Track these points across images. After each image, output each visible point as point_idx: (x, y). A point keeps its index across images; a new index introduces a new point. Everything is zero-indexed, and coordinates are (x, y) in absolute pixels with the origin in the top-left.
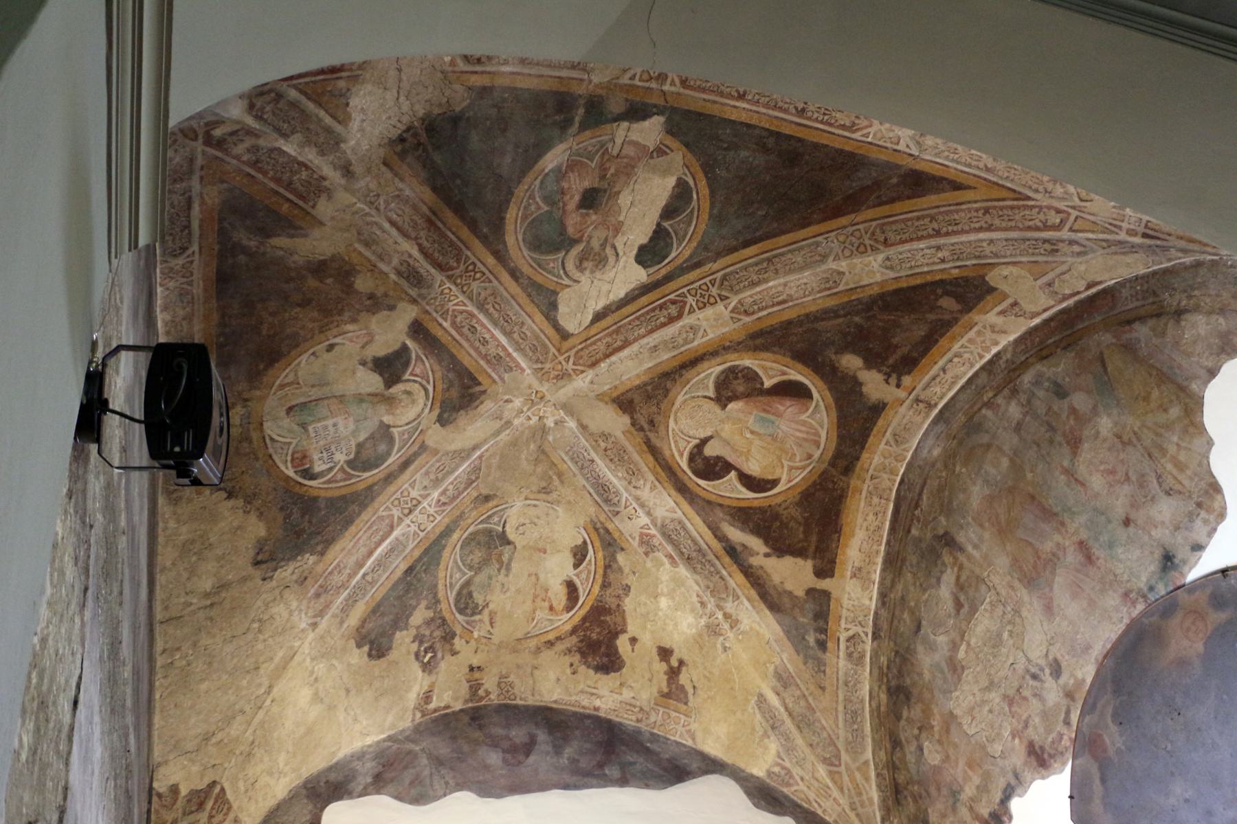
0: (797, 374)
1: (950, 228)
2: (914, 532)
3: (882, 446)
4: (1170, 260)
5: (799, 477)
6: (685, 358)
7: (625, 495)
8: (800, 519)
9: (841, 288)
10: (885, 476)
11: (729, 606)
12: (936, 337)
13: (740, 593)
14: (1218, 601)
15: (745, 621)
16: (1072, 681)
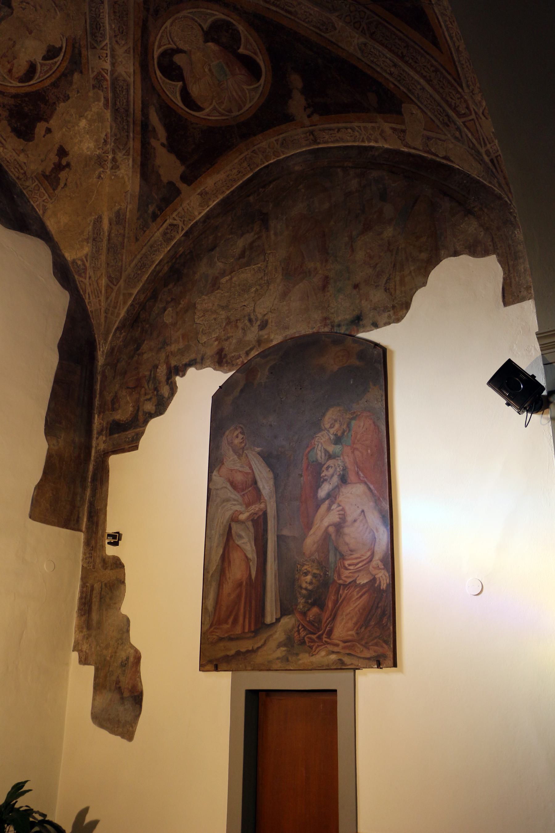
1: (411, 61)
2: (251, 199)
3: (273, 140)
4: (490, 183)
7: (107, 41)
10: (261, 156)
11: (120, 156)
13: (131, 152)
14: (361, 355)
15: (122, 171)
16: (266, 337)
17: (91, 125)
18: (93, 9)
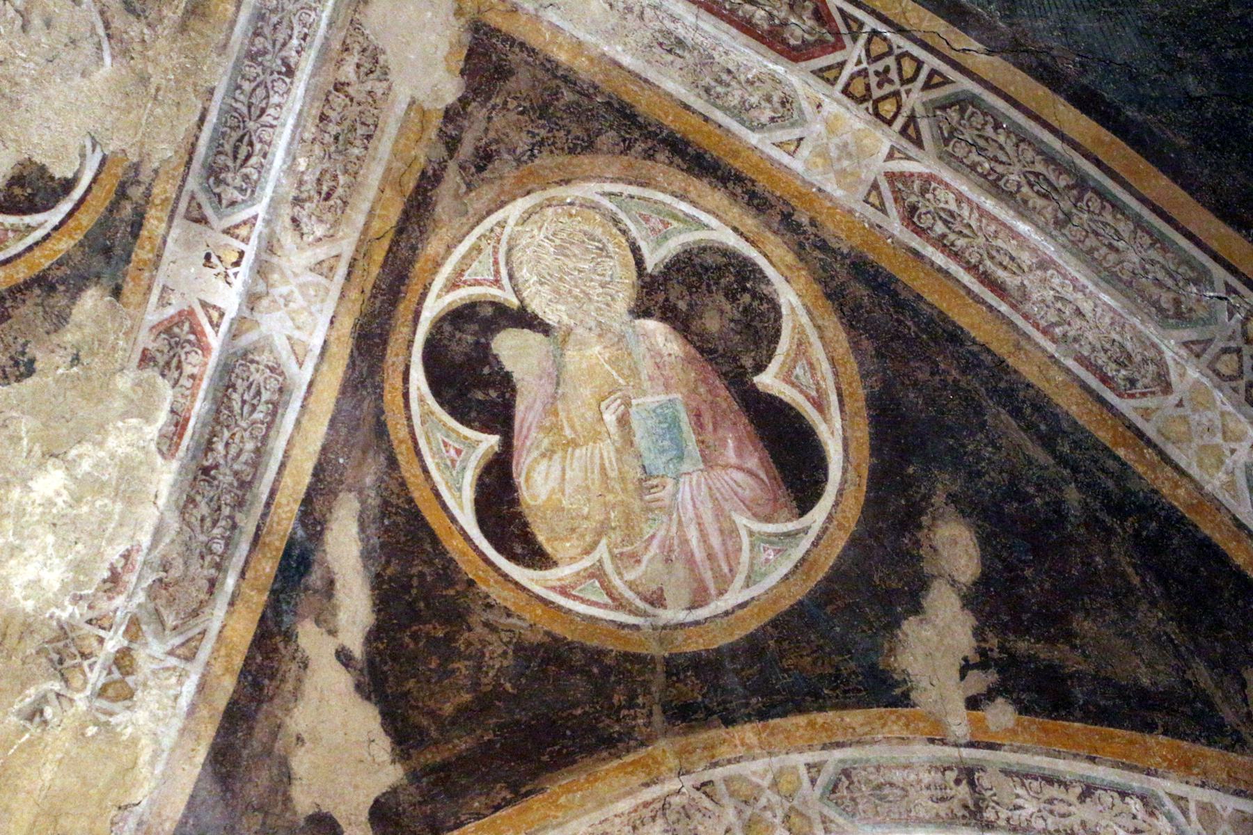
0: (838, 438)
3: (799, 760)
5: (589, 606)
6: (699, 138)
7: (260, 209)
8: (487, 680)
9: (1125, 406)
10: (730, 816)
11: (153, 652)
12: (1159, 718)
13: (204, 654)
15: (141, 716)
17: (78, 500)
18: (247, 86)
